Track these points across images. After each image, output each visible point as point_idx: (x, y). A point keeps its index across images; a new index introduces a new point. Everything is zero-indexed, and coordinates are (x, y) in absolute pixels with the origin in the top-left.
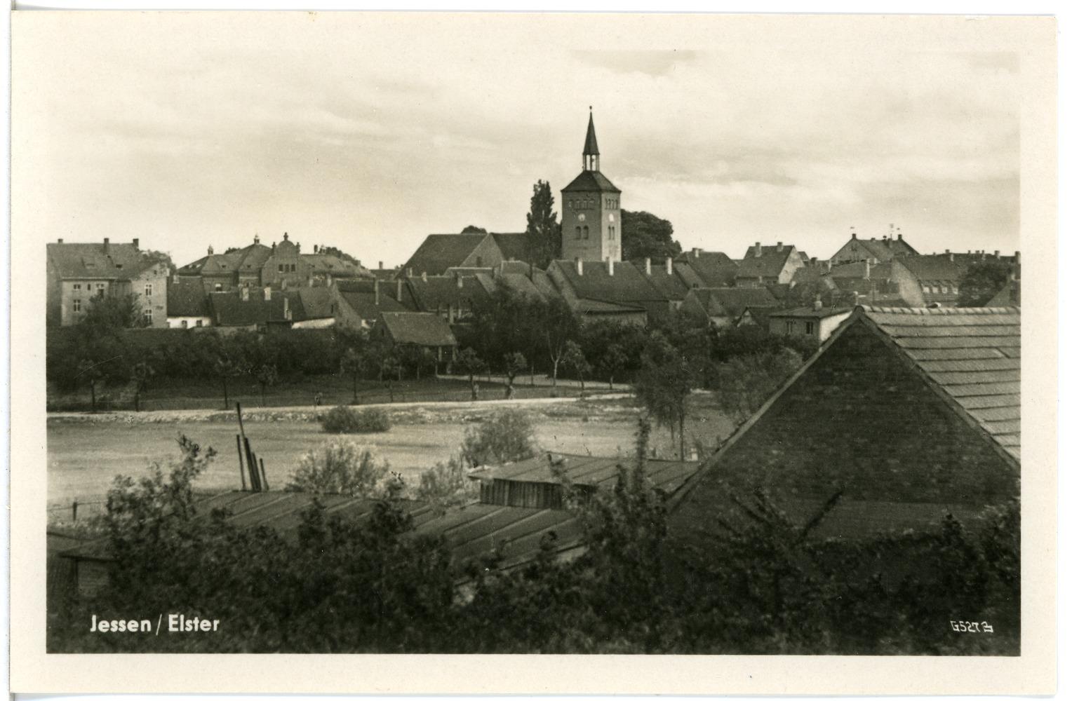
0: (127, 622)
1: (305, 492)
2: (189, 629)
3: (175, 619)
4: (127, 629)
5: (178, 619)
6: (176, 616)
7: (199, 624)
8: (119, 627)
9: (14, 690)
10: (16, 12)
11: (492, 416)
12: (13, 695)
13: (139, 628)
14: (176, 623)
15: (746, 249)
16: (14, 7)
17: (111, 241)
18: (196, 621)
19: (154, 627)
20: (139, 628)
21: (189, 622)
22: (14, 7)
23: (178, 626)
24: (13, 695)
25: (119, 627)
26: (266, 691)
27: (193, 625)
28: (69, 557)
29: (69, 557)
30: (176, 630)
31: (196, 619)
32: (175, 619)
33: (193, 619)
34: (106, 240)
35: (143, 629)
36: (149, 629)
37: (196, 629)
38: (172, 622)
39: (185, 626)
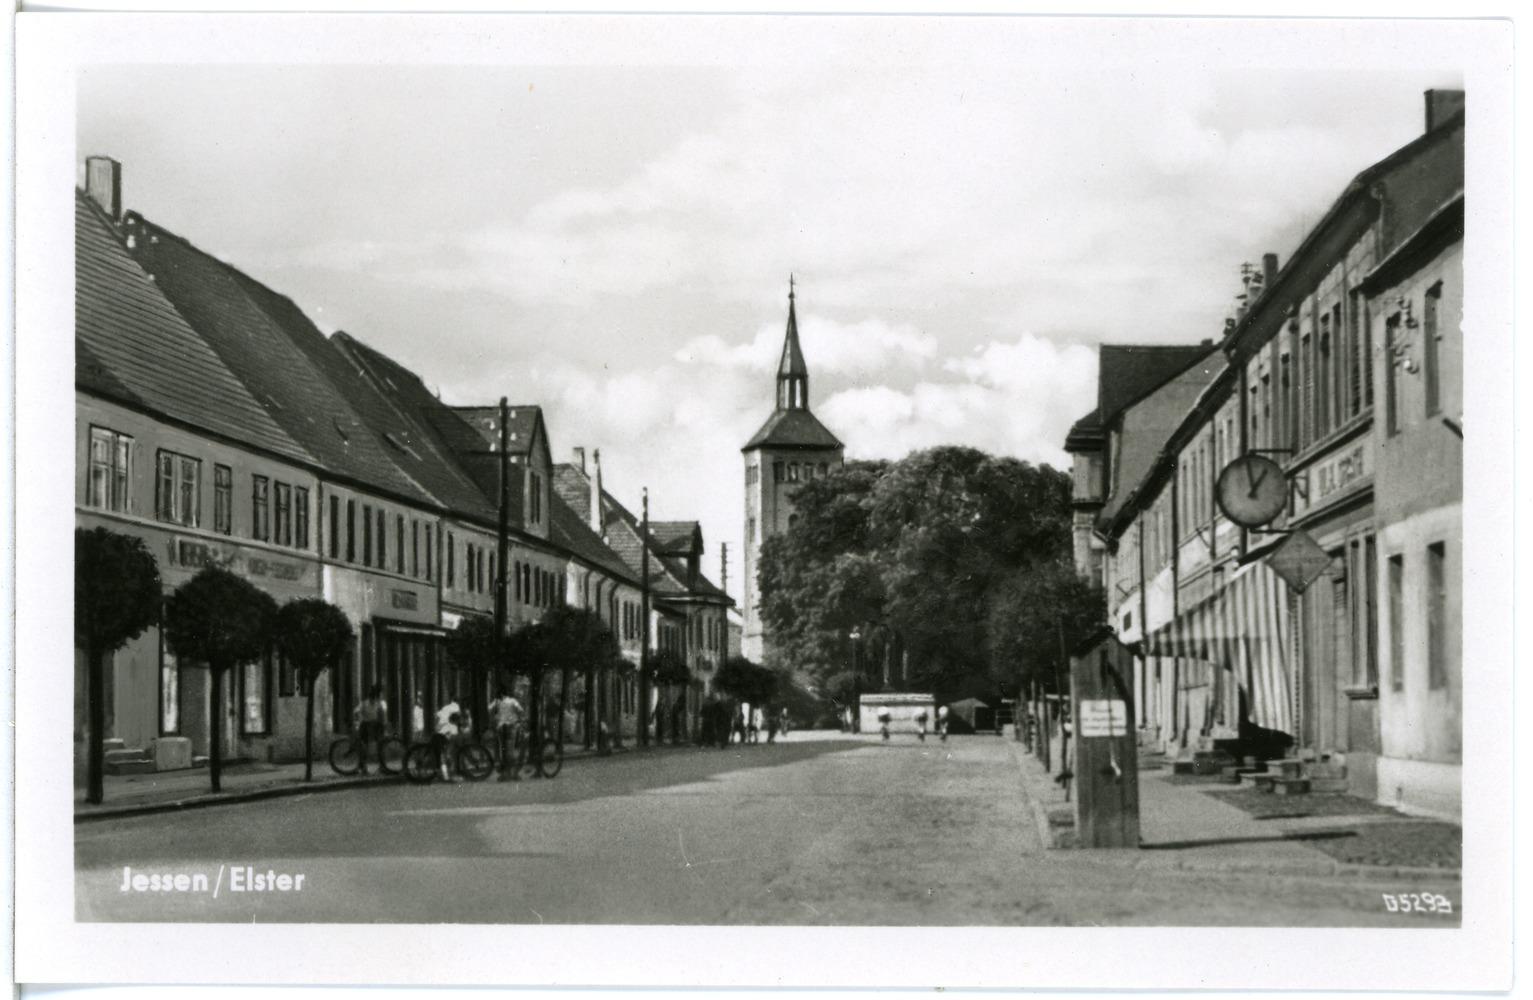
0: (174, 876)
1: (916, 720)
2: (260, 887)
3: (239, 874)
4: (131, 887)
5: (245, 874)
6: (241, 869)
7: (275, 882)
8: (162, 883)
9: (18, 981)
10: (20, 14)
11: (144, 547)
12: (20, 988)
13: (293, 885)
14: (242, 879)
15: (72, 195)
16: (20, 8)
17: (510, 403)
18: (271, 875)
19: (212, 884)
20: (293, 885)
21: (260, 878)
22: (20, 8)
23: (244, 883)
24: (20, 988)
25: (162, 883)
26: (406, 982)
27: (267, 882)
28: (161, 771)
29: (161, 771)
30: (241, 889)
31: (271, 873)
32: (239, 874)
33: (266, 874)
34: (504, 401)
35: (196, 888)
36: (205, 888)
37: (271, 888)
38: (235, 878)
39: (254, 883)
